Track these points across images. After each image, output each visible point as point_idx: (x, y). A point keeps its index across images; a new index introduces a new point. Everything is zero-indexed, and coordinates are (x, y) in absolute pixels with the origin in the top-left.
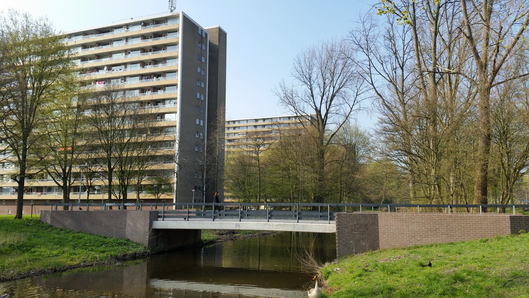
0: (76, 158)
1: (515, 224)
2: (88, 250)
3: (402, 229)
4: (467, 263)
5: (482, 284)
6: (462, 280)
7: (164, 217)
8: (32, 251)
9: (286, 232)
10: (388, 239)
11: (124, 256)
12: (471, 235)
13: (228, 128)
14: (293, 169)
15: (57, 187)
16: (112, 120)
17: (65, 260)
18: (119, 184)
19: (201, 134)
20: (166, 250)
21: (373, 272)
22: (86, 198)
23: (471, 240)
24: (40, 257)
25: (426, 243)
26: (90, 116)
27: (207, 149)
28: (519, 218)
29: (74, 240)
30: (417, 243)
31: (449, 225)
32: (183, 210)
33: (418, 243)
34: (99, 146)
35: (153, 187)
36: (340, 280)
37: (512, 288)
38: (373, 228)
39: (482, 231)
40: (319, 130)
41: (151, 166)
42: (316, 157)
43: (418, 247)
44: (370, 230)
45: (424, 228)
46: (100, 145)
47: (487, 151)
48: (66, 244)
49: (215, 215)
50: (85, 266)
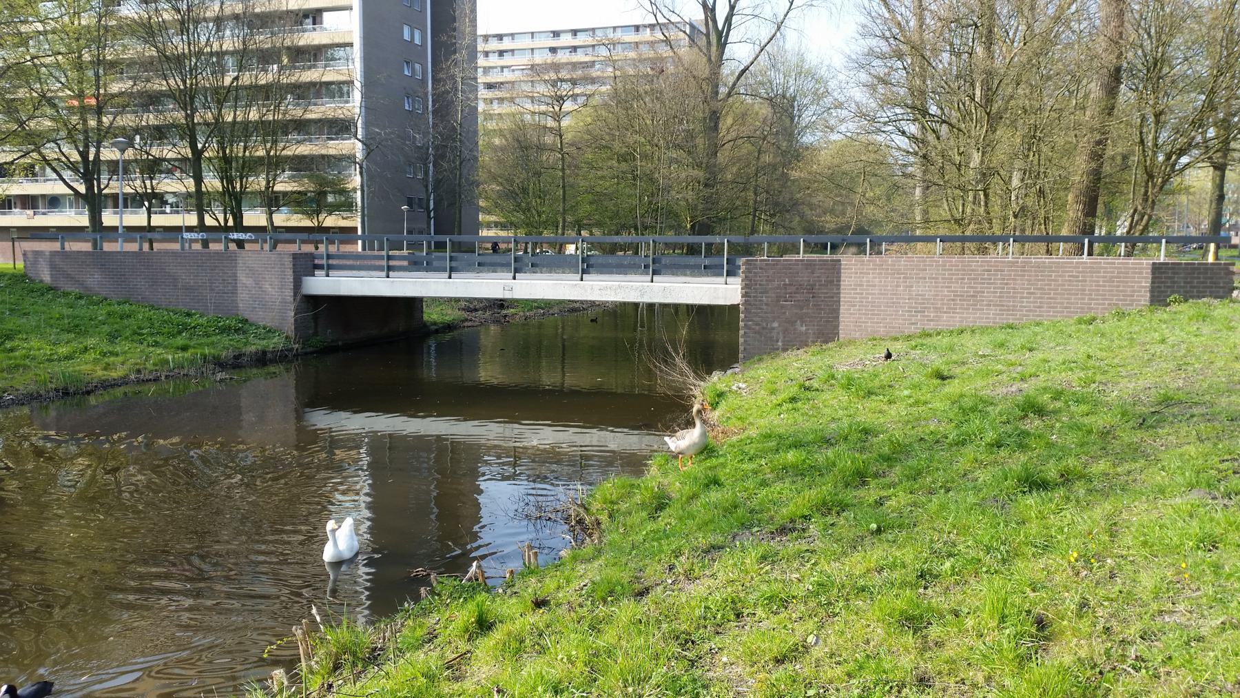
0: (111, 124)
1: (1162, 282)
2: (145, 343)
3: (895, 294)
4: (1049, 372)
5: (1086, 420)
6: (1040, 412)
7: (330, 267)
8: (6, 348)
9: (625, 304)
10: (859, 318)
11: (236, 357)
12: (1056, 307)
13: (486, 54)
14: (645, 156)
15: (72, 198)
16: (191, 27)
17: (89, 367)
18: (221, 190)
19: (417, 66)
20: (340, 343)
21: (822, 391)
22: (145, 224)
23: (1056, 319)
24: (27, 362)
25: (950, 326)
26: (136, 17)
27: (433, 106)
28: (1173, 268)
29: (111, 320)
30: (928, 325)
31: (1007, 284)
32: (376, 253)
33: (930, 327)
34: (164, 95)
35: (304, 197)
36: (747, 410)
37: (1160, 431)
38: (827, 293)
39: (1084, 299)
40: (710, 60)
41: (295, 147)
42: (698, 127)
43: (930, 335)
44: (820, 297)
45: (948, 291)
46: (166, 91)
47: (1110, 110)
48: (90, 330)
49: (454, 264)
50: (140, 382)
